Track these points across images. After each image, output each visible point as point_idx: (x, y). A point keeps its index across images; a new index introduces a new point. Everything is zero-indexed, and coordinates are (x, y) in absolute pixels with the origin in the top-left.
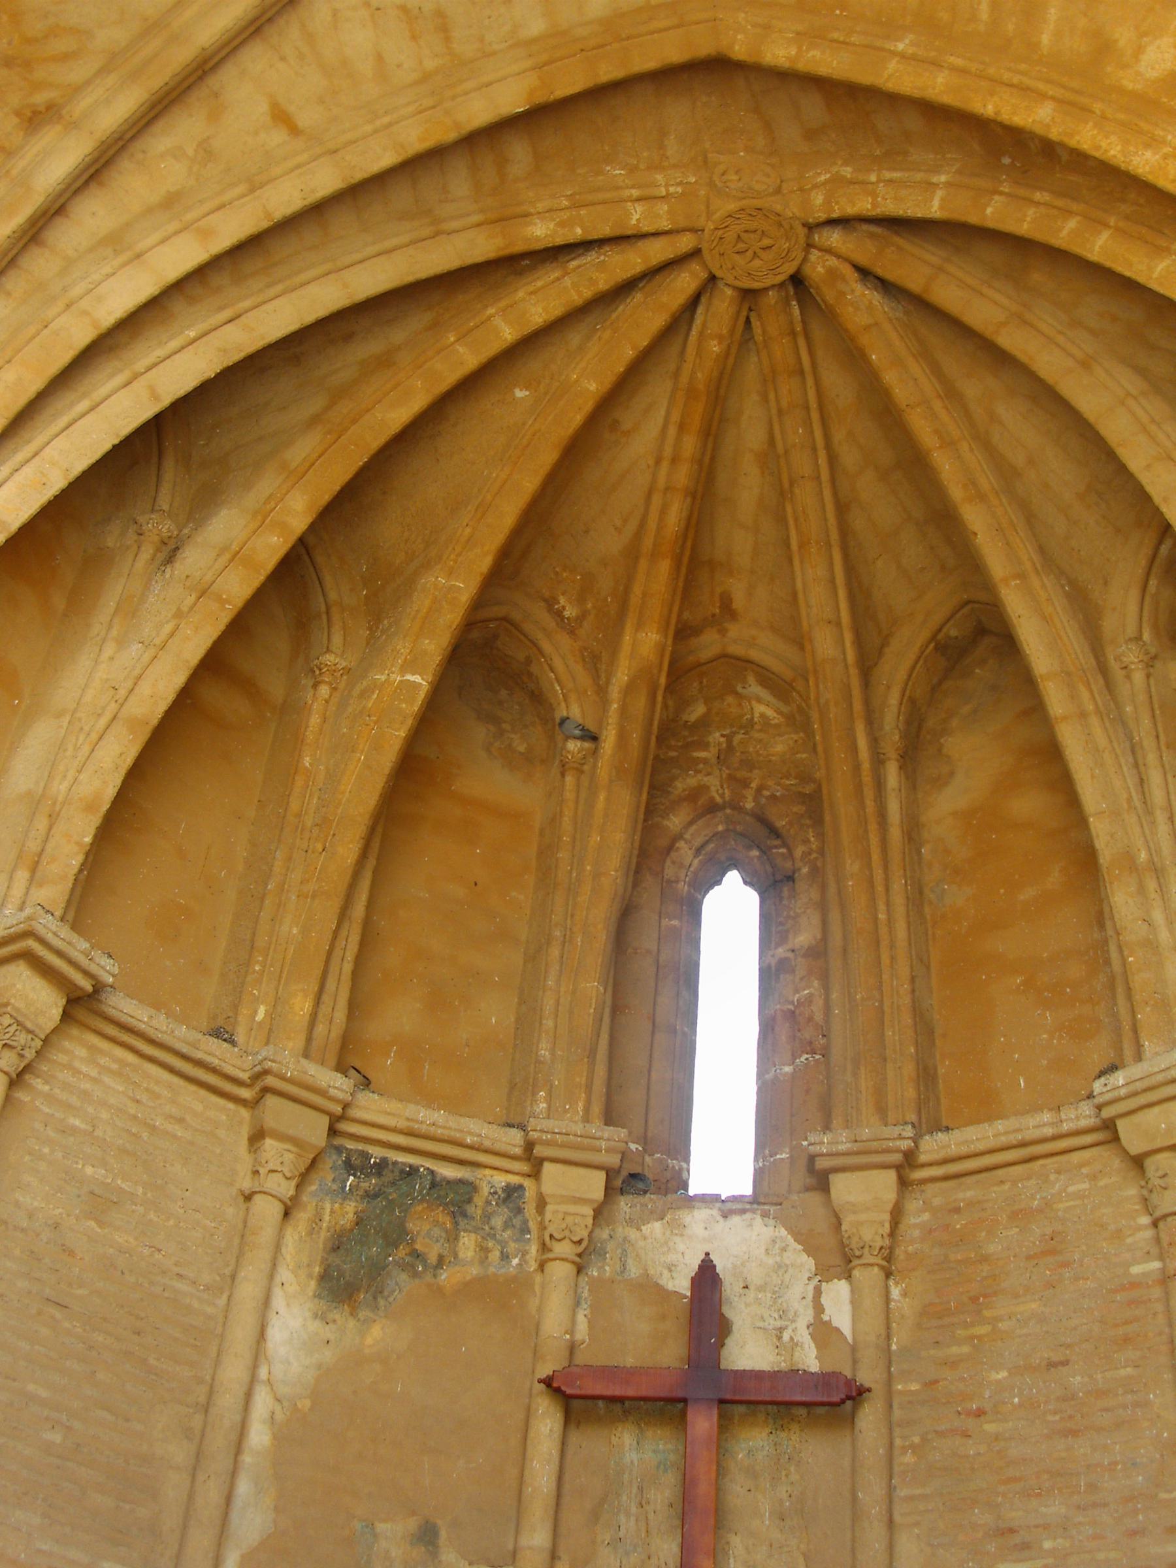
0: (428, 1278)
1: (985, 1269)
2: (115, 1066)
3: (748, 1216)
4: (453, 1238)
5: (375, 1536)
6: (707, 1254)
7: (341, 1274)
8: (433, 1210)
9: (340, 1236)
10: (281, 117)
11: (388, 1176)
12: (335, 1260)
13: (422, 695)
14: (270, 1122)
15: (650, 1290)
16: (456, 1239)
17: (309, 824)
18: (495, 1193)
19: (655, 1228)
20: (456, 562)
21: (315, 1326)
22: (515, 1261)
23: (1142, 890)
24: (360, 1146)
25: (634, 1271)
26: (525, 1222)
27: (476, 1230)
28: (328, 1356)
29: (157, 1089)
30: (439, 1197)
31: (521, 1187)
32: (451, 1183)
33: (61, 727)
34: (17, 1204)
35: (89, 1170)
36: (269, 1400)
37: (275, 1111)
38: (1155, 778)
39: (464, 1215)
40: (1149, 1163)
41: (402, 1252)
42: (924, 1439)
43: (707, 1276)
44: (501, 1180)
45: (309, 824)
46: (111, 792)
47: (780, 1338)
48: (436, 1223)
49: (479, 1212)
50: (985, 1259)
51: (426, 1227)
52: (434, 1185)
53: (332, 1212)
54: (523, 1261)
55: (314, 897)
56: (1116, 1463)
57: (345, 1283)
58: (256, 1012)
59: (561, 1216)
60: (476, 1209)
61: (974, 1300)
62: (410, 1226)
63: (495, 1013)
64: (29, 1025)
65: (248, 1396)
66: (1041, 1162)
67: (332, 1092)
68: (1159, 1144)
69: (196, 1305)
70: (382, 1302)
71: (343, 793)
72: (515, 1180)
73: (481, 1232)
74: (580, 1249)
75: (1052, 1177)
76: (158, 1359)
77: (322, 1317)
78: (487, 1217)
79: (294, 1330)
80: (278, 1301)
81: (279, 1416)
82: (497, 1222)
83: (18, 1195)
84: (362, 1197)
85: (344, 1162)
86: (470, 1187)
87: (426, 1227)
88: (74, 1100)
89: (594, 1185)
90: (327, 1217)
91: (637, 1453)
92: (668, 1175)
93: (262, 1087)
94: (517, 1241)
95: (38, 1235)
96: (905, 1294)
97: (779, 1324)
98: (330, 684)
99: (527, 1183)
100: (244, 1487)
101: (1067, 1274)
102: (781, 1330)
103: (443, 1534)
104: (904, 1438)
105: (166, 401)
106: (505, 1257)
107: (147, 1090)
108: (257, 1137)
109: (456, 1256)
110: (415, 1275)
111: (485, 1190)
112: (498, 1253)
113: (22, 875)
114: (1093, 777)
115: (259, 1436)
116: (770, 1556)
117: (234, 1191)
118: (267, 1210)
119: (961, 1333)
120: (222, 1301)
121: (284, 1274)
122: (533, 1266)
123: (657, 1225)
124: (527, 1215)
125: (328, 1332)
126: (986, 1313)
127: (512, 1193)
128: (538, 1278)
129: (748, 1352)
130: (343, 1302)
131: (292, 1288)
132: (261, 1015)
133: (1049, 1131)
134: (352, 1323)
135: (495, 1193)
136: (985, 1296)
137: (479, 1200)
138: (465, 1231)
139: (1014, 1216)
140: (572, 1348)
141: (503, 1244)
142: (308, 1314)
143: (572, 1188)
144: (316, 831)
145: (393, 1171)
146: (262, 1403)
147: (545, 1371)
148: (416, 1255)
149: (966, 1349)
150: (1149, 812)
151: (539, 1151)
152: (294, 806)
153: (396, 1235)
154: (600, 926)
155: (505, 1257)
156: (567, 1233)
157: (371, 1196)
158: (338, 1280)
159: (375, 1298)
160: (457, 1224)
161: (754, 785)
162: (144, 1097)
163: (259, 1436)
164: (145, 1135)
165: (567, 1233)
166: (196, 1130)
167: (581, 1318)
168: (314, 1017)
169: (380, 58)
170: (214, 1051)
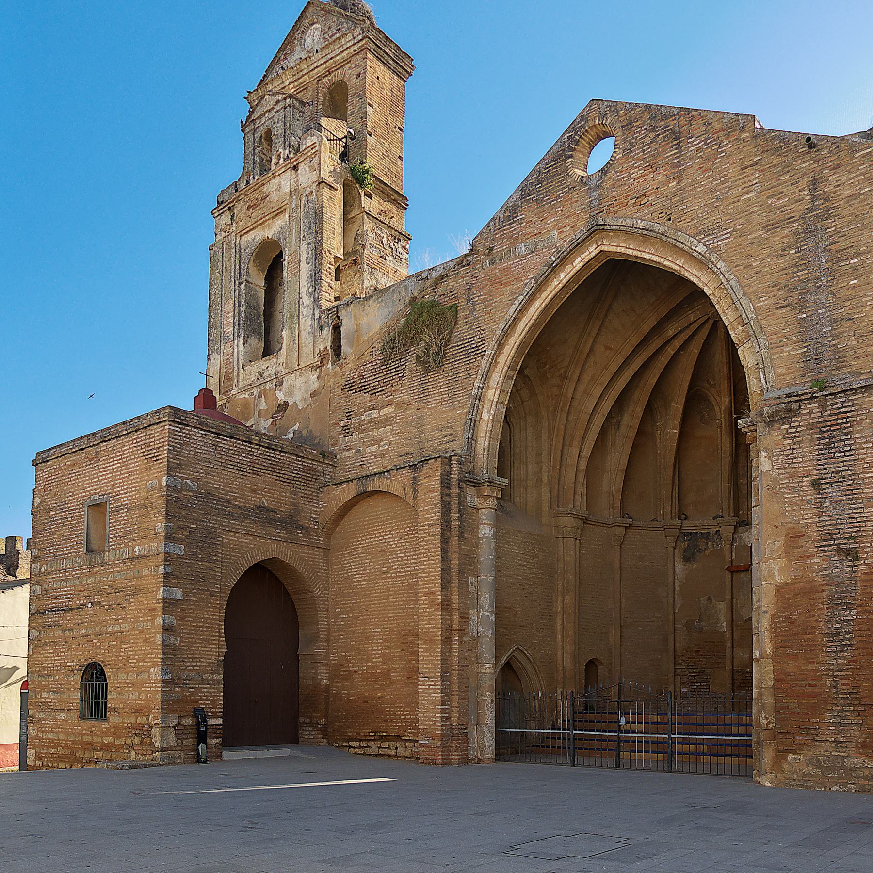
57: (687, 559)
79: (679, 567)
80: (676, 564)
115: (677, 588)
121: (676, 559)
146: (677, 582)
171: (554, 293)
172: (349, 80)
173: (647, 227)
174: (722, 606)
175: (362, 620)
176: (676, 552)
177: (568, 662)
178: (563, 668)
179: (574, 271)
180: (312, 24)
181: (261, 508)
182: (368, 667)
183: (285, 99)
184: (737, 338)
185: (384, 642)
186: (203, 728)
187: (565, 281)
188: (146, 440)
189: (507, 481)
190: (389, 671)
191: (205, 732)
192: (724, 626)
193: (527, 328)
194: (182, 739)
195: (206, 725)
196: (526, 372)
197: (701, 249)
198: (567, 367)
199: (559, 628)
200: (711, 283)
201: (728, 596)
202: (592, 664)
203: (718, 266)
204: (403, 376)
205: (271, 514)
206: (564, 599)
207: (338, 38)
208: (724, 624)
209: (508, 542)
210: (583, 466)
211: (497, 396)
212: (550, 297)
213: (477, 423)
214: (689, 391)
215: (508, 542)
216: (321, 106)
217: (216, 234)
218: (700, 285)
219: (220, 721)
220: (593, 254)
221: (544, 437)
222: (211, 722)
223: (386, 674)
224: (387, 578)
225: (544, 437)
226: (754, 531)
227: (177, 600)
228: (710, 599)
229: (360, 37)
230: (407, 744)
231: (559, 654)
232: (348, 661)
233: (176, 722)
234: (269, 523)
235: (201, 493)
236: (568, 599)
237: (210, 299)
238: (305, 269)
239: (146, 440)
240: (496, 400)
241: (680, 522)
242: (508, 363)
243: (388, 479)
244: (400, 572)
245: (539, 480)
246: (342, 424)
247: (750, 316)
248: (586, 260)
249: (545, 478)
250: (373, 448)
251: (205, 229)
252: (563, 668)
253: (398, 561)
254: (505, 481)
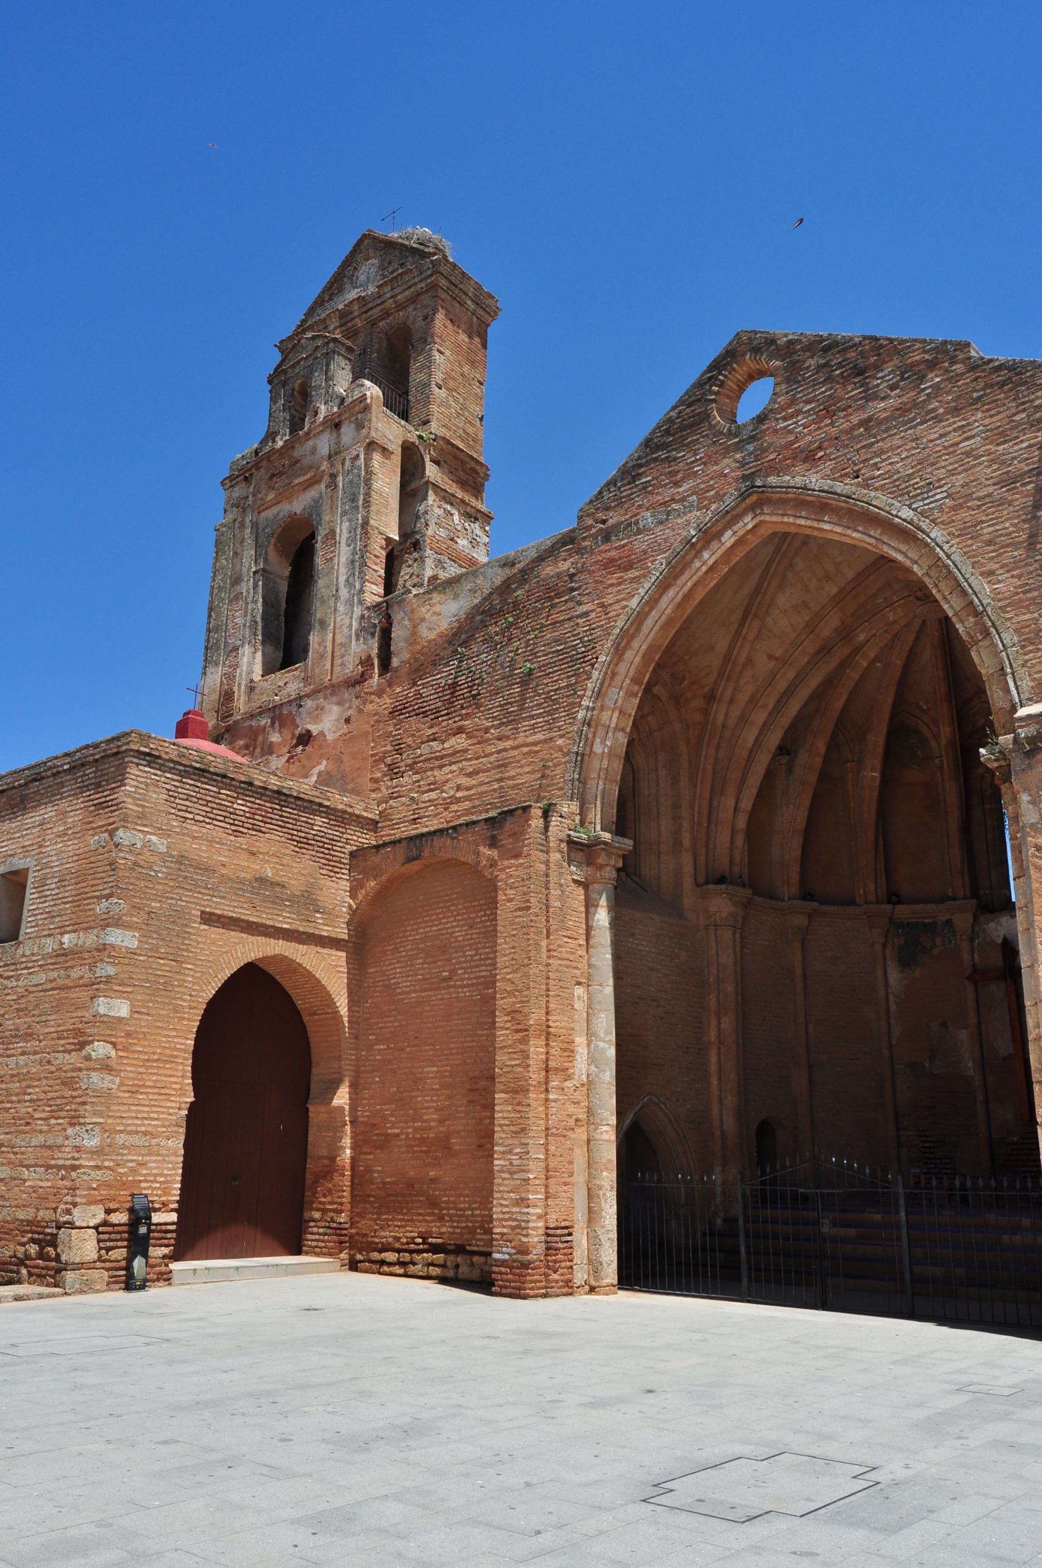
10: (771, 657)
13: (878, 781)
19: (992, 925)
44: (944, 919)
46: (800, 853)
57: (906, 962)
65: (887, 1000)
79: (894, 975)
80: (889, 971)
82: (946, 931)
89: (969, 917)
100: (892, 1022)
106: (950, 942)
115: (893, 1008)
121: (889, 962)
140: (974, 965)
143: (963, 921)
146: (892, 999)
167: (976, 956)
168: (876, 888)
169: (792, 625)
171: (695, 578)
172: (414, 322)
173: (826, 488)
174: (963, 1035)
175: (408, 1053)
176: (888, 952)
177: (729, 1123)
178: (723, 1132)
179: (724, 548)
180: (368, 260)
181: (262, 881)
182: (416, 1129)
183: (328, 343)
184: (968, 633)
185: (442, 1087)
186: (143, 1230)
187: (711, 562)
188: (95, 778)
189: (630, 842)
190: (447, 1137)
191: (146, 1238)
192: (969, 1066)
193: (657, 627)
194: (108, 1249)
195: (150, 1224)
196: (656, 690)
197: (906, 513)
198: (715, 683)
199: (713, 1068)
200: (924, 559)
201: (973, 1019)
202: (765, 1131)
203: (933, 535)
204: (479, 694)
205: (278, 889)
206: (719, 1024)
207: (401, 275)
208: (970, 1064)
209: (633, 934)
210: (742, 823)
211: (614, 720)
212: (689, 584)
213: (586, 758)
214: (892, 718)
215: (633, 934)
216: (375, 355)
217: (225, 511)
218: (908, 563)
219: (174, 1217)
220: (750, 526)
221: (684, 781)
222: (157, 1218)
223: (444, 1141)
224: (448, 987)
225: (684, 781)
226: (1020, 916)
227: (120, 1019)
228: (944, 1025)
229: (429, 272)
230: (475, 1259)
231: (715, 1111)
232: (384, 1118)
233: (100, 1216)
234: (273, 902)
235: (173, 857)
236: (728, 1022)
237: (212, 595)
238: (344, 553)
239: (95, 778)
240: (613, 725)
241: (889, 907)
242: (631, 674)
243: (454, 838)
244: (469, 979)
245: (677, 843)
246: (389, 760)
247: (985, 602)
248: (740, 533)
249: (687, 841)
250: (433, 795)
251: (213, 507)
252: (723, 1132)
253: (466, 962)
254: (628, 843)
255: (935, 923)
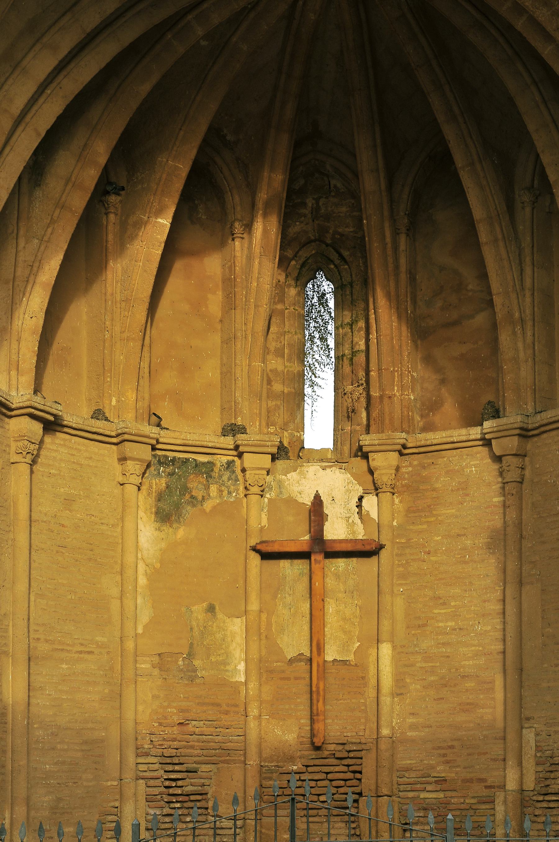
0: (200, 507)
1: (435, 494)
2: (62, 443)
3: (334, 468)
4: (207, 488)
5: (192, 612)
6: (317, 491)
7: (164, 510)
8: (197, 477)
9: (161, 494)
11: (177, 465)
12: (160, 504)
14: (128, 454)
15: (291, 502)
16: (209, 488)
17: (118, 299)
18: (223, 465)
19: (293, 476)
20: (176, 151)
21: (156, 533)
22: (234, 494)
23: (514, 333)
24: (164, 453)
25: (285, 496)
26: (237, 476)
27: (216, 483)
28: (163, 545)
29: (79, 447)
30: (199, 471)
31: (233, 461)
32: (203, 464)
33: (9, 290)
34: (40, 512)
35: (62, 490)
36: (144, 566)
37: (130, 449)
38: (528, 271)
39: (211, 477)
40: (503, 458)
41: (187, 496)
42: (407, 562)
43: (318, 501)
44: (225, 459)
45: (118, 299)
47: (348, 521)
48: (199, 482)
49: (217, 475)
50: (434, 490)
51: (196, 485)
52: (196, 465)
53: (156, 484)
54: (237, 493)
55: (128, 340)
56: (481, 575)
57: (165, 516)
58: (111, 401)
59: (253, 475)
60: (215, 474)
61: (429, 506)
62: (189, 485)
63: (211, 371)
64: (33, 441)
66: (460, 450)
67: (152, 435)
68: (508, 453)
69: (110, 533)
70: (182, 519)
71: (134, 285)
72: (230, 458)
73: (219, 483)
74: (262, 489)
75: (465, 457)
76: (100, 558)
77: (159, 529)
78: (220, 476)
79: (147, 535)
80: (141, 526)
81: (148, 571)
82: (225, 478)
83: (39, 508)
84: (168, 476)
85: (158, 461)
86: (211, 464)
87: (196, 485)
88: (51, 462)
90: (154, 487)
91: (290, 569)
92: (295, 439)
93: (121, 440)
94: (234, 485)
95: (50, 522)
96: (401, 502)
97: (348, 515)
98: (114, 213)
99: (236, 459)
101: (468, 499)
102: (349, 517)
103: (217, 608)
104: (399, 561)
105: (43, 134)
106: (230, 493)
107: (76, 449)
108: (123, 459)
109: (209, 495)
110: (194, 506)
111: (219, 464)
112: (227, 492)
113: (13, 373)
114: (497, 275)
115: (142, 581)
116: (346, 607)
117: (116, 483)
118: (131, 489)
119: (424, 520)
120: (119, 529)
122: (242, 495)
123: (293, 474)
124: (237, 473)
125: (162, 535)
126: (434, 512)
127: (230, 464)
128: (245, 500)
129: (335, 530)
130: (166, 522)
131: (145, 518)
132: (114, 402)
133: (464, 438)
134: (171, 530)
135: (223, 465)
136: (435, 505)
137: (216, 470)
138: (212, 484)
139: (447, 472)
141: (228, 487)
142: (153, 529)
144: (123, 304)
145: (179, 462)
146: (141, 567)
147: (253, 542)
148: (192, 497)
149: (425, 526)
150: (523, 289)
151: (241, 449)
152: (109, 290)
153: (185, 489)
154: (260, 334)
155: (230, 493)
156: (256, 482)
157: (171, 474)
158: (163, 513)
159: (179, 518)
160: (208, 481)
161: (331, 231)
162: (74, 452)
163: (142, 581)
164: (79, 469)
165: (256, 482)
166: (97, 461)
170: (99, 425)
255: (211, 464)
